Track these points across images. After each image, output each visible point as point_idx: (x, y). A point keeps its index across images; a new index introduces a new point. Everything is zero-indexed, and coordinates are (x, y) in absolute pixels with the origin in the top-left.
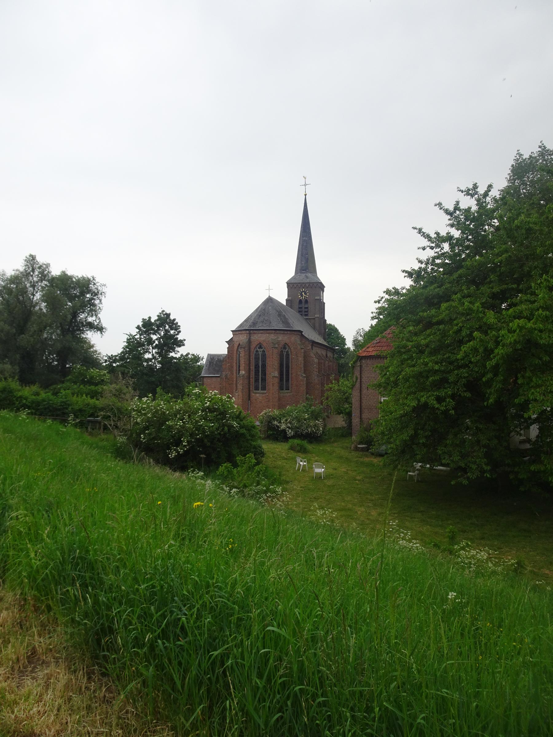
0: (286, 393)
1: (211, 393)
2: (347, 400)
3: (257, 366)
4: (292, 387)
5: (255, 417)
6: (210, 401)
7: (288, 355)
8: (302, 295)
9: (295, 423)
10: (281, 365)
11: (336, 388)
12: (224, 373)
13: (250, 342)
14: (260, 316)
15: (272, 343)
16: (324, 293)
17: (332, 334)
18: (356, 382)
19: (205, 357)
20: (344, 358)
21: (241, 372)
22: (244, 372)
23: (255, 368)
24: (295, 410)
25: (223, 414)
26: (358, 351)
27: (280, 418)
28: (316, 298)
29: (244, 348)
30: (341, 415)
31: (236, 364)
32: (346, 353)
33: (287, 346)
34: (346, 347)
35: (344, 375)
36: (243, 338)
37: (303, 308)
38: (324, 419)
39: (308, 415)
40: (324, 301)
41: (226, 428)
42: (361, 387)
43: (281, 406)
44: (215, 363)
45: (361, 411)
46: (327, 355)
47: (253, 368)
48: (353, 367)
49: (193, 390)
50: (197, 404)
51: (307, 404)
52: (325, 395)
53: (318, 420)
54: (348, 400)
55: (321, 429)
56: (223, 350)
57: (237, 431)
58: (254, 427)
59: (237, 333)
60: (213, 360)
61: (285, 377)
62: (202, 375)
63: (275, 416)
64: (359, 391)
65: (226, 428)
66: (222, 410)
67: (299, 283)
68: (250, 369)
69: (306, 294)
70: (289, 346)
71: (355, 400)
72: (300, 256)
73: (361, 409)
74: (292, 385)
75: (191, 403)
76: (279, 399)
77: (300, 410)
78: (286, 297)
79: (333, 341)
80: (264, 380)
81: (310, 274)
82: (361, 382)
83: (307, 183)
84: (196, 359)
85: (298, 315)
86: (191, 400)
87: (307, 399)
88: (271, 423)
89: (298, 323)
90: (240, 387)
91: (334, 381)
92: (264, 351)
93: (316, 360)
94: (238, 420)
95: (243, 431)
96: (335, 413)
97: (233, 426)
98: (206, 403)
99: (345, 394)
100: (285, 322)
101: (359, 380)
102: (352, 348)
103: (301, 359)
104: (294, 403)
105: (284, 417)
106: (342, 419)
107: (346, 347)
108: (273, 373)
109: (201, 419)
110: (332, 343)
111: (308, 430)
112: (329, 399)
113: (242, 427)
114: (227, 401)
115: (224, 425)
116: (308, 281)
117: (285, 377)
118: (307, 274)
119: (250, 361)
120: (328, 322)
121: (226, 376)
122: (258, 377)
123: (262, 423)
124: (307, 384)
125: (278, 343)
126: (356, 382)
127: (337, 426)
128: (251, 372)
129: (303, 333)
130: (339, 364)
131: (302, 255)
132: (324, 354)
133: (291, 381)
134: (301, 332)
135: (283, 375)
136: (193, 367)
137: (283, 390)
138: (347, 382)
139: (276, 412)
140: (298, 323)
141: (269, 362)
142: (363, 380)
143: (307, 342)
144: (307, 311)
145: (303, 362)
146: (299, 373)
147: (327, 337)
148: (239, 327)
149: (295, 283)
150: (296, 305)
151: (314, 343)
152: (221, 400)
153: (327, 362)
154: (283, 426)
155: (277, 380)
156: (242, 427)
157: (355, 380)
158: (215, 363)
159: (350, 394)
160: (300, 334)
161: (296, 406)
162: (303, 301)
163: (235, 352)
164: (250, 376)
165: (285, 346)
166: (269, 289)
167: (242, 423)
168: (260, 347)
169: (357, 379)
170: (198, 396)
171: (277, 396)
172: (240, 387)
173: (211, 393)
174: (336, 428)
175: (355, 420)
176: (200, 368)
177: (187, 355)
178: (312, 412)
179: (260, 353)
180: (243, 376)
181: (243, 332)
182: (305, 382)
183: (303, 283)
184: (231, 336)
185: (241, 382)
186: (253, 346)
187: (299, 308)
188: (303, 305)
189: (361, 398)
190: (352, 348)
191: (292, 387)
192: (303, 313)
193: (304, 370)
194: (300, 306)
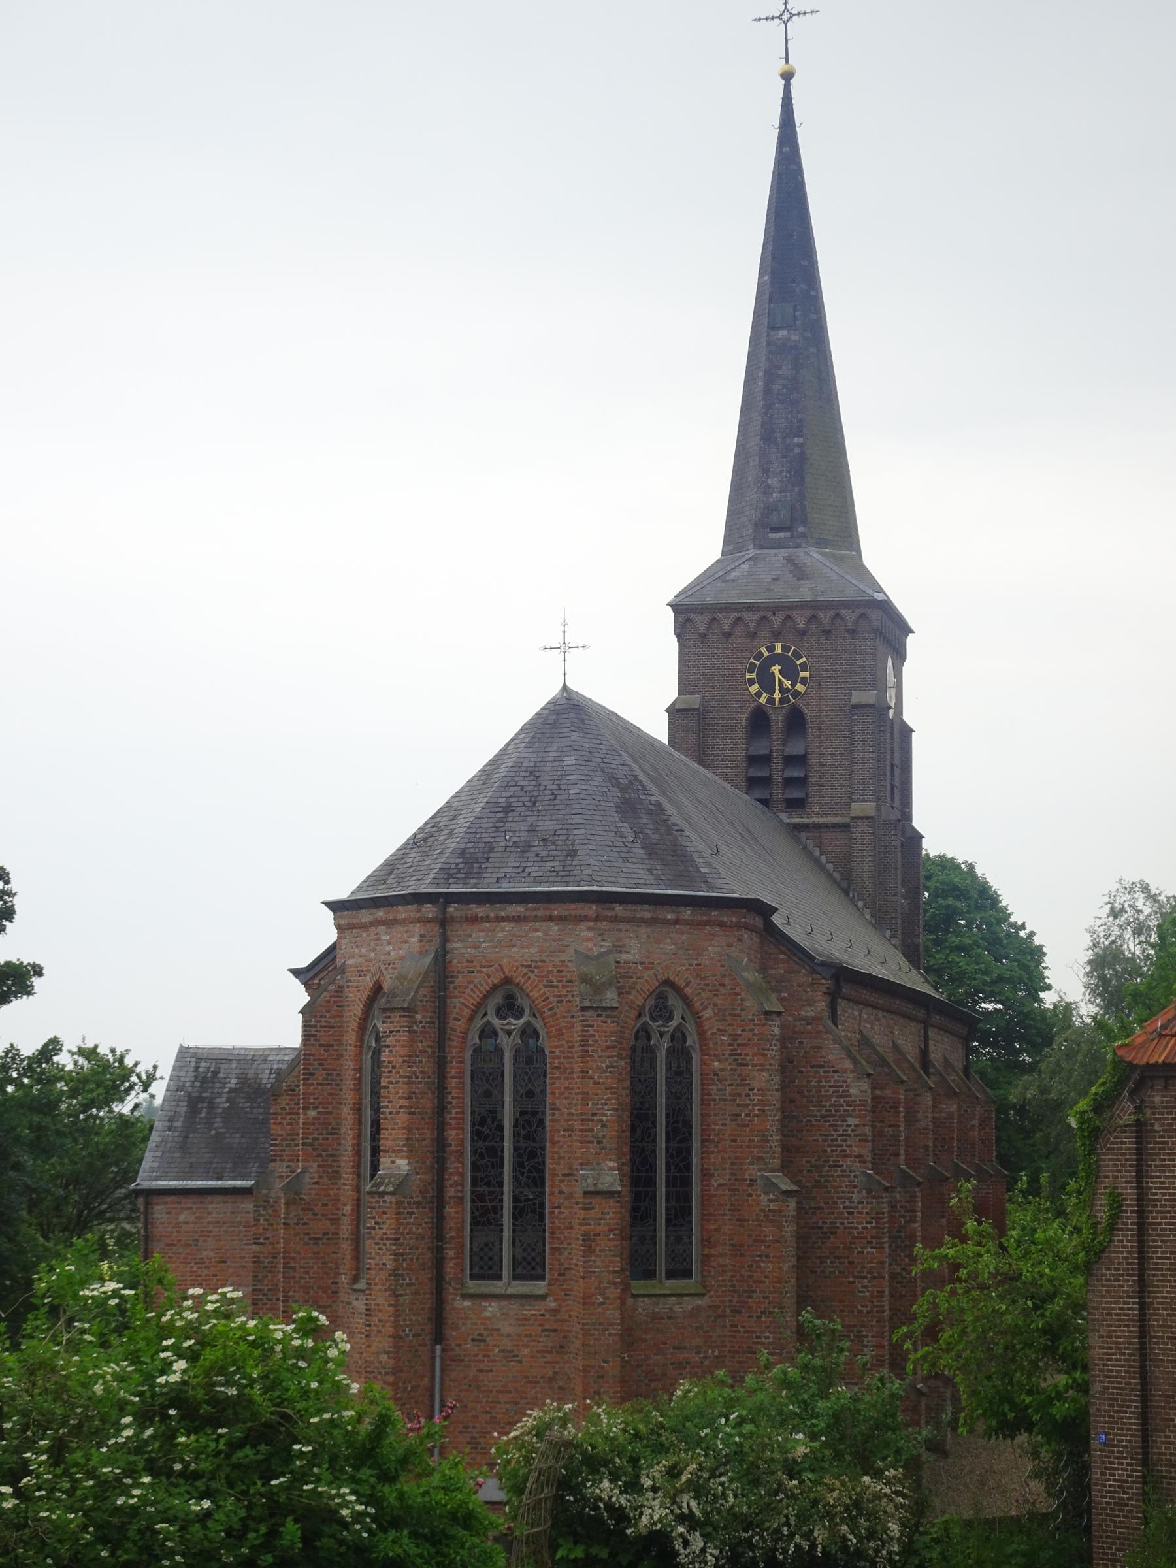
0: (672, 1300)
1: (200, 1301)
2: (1058, 1341)
3: (486, 1127)
4: (706, 1259)
5: (478, 1447)
6: (192, 1357)
7: (680, 1052)
8: (767, 682)
9: (730, 1494)
10: (639, 1121)
11: (989, 1263)
12: (280, 1168)
13: (441, 975)
14: (508, 810)
15: (585, 979)
16: (907, 669)
17: (951, 915)
18: (1112, 1227)
19: (165, 1071)
20: (1032, 1068)
21: (385, 1161)
22: (403, 1165)
23: (477, 1135)
24: (730, 1404)
25: (272, 1434)
26: (1126, 1030)
27: (634, 1461)
28: (858, 697)
29: (409, 1011)
30: (1023, 1438)
31: (358, 1109)
32: (1048, 1040)
33: (673, 1001)
34: (1049, 999)
35: (1034, 1179)
36: (401, 952)
37: (777, 761)
38: (913, 1466)
39: (813, 1437)
40: (907, 717)
41: (291, 1530)
42: (1142, 1259)
43: (638, 1384)
44: (222, 1103)
45: (1145, 1417)
46: (924, 1054)
47: (460, 1135)
48: (1094, 1135)
49: (84, 1283)
50: (108, 1374)
51: (806, 1368)
52: (921, 1307)
53: (877, 1474)
54: (1064, 1345)
55: (894, 1528)
56: (272, 1021)
57: (360, 1549)
58: (466, 1519)
59: (365, 916)
60: (211, 1081)
61: (661, 1189)
62: (144, 1181)
63: (603, 1447)
64: (1129, 1284)
65: (291, 1530)
66: (267, 1410)
67: (751, 607)
68: (441, 1143)
69: (790, 672)
70: (687, 1002)
71: (1106, 1342)
72: (754, 443)
73: (1144, 1398)
74: (706, 1242)
75: (69, 1364)
76: (629, 1336)
77: (761, 1409)
78: (671, 693)
79: (962, 961)
80: (531, 1212)
81: (815, 554)
82: (1142, 1227)
84: (107, 1076)
85: (744, 800)
86: (74, 1347)
87: (802, 1334)
88: (576, 1489)
89: (743, 857)
90: (380, 1258)
91: (970, 1225)
92: (529, 1033)
93: (859, 1090)
94: (365, 1473)
95: (398, 1544)
96: (981, 1427)
97: (332, 1515)
98: (166, 1368)
99: (1041, 1301)
100: (667, 848)
101: (1129, 1217)
102: (1087, 1010)
103: (764, 1079)
104: (719, 1362)
105: (661, 1449)
106: (1030, 1466)
107: (1049, 999)
108: (587, 1168)
109: (131, 1472)
110: (959, 979)
111: (808, 1536)
112: (946, 1335)
113: (388, 1521)
114: (300, 1353)
115: (276, 1509)
116: (804, 592)
117: (661, 1189)
118: (800, 553)
119: (441, 1090)
120: (932, 847)
121: (293, 1189)
122: (494, 1190)
123: (518, 1490)
124: (802, 1238)
125: (622, 979)
126: (1112, 1227)
127: (997, 1507)
128: (452, 1165)
129: (777, 919)
130: (1002, 1108)
131: (767, 437)
132: (909, 1044)
133: (705, 1217)
134: (763, 910)
135: (651, 1182)
136: (87, 1130)
137: (650, 1274)
138: (1053, 1229)
139: (611, 1420)
140: (743, 857)
142: (1154, 1216)
143: (803, 976)
144: (802, 782)
145: (775, 1098)
146: (752, 1171)
147: (924, 939)
148: (374, 880)
149: (727, 608)
150: (734, 746)
151: (844, 981)
152: (262, 1344)
153: (928, 1099)
154: (653, 1513)
155: (611, 1215)
156: (388, 1521)
157: (1103, 1217)
158: (222, 1103)
159: (1078, 1307)
160: (758, 922)
161: (737, 1379)
162: (777, 719)
163: (351, 1037)
164: (441, 1189)
165: (664, 997)
166: (564, 648)
167: (389, 1493)
168: (510, 1007)
169: (1115, 1217)
170: (116, 1322)
171: (613, 1314)
172: (380, 1258)
173: (200, 1301)
174: (990, 1523)
175: (1113, 1475)
176: (131, 1132)
177: (52, 1047)
178: (837, 1418)
179: (508, 1044)
180: (401, 1186)
181: (403, 912)
182: (789, 1229)
183: (775, 608)
184: (323, 933)
185: (388, 1226)
186: (461, 1003)
187: (752, 760)
188: (775, 744)
189: (1143, 1333)
190: (1087, 1010)
191: (706, 1259)
192: (778, 793)
193: (786, 1149)
194: (760, 748)
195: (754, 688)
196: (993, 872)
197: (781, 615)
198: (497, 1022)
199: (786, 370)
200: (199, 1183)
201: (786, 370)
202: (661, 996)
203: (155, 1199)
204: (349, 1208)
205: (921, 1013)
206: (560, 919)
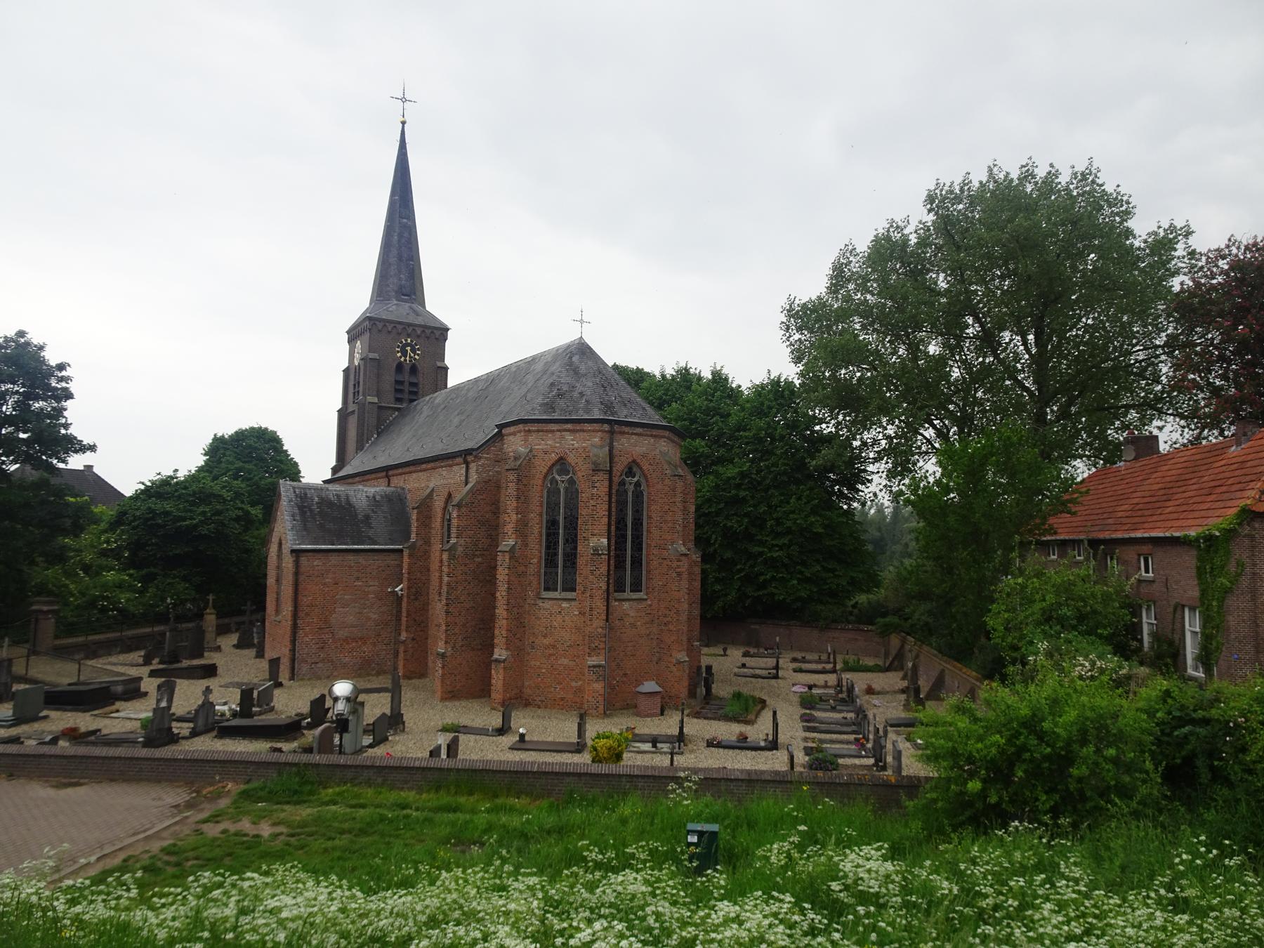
3: (552, 524)
7: (638, 495)
8: (404, 353)
37: (407, 384)
67: (400, 323)
69: (413, 351)
80: (571, 558)
108: (595, 540)
141: (654, 512)
179: (562, 487)
183: (410, 325)
187: (397, 382)
196: (280, 434)
198: (557, 477)
199: (406, 235)
201: (406, 235)
202: (630, 468)
204: (535, 561)
206: (655, 436)
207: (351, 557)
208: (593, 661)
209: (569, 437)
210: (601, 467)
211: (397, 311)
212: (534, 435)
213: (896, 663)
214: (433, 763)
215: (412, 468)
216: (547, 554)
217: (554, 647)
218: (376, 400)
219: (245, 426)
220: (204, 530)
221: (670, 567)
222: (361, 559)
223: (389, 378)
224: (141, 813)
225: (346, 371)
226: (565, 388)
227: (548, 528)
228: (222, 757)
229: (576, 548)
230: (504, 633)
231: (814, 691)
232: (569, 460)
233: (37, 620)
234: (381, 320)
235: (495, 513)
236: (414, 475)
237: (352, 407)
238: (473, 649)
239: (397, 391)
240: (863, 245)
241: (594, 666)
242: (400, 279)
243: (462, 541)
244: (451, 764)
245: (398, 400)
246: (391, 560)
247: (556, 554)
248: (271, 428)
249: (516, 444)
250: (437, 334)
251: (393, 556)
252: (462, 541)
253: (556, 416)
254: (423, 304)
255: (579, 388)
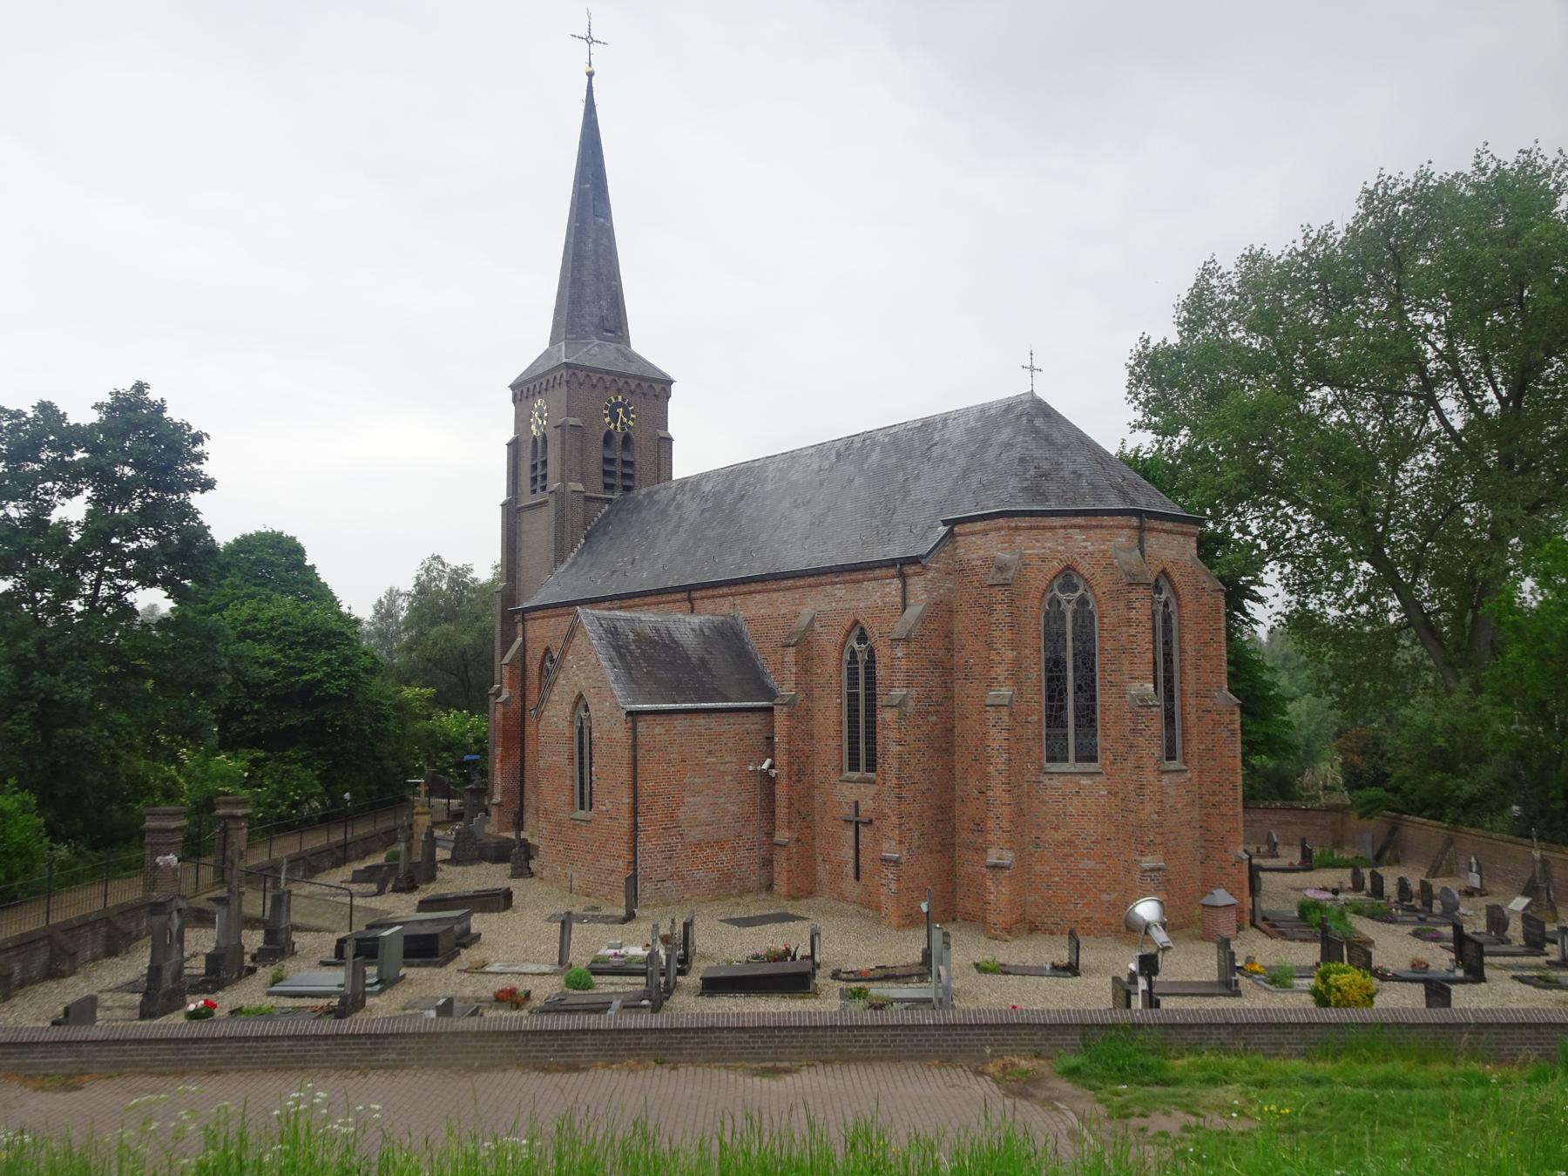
3: (1055, 666)
67: (608, 373)
69: (626, 414)
80: (1087, 717)
83: (585, 34)
92: (1083, 602)
179: (1069, 610)
183: (621, 375)
187: (607, 461)
194: (609, 455)
195: (607, 419)
197: (623, 380)
200: (690, 705)
203: (640, 718)
205: (685, 595)
207: (700, 721)
208: (1148, 862)
209: (1078, 536)
210: (1141, 579)
211: (596, 354)
212: (1024, 534)
213: (1388, 854)
214: (1122, 1016)
215: (758, 587)
216: (1050, 708)
217: (1070, 843)
218: (580, 487)
219: (250, 530)
220: (332, 688)
221: (1217, 723)
222: (713, 722)
223: (596, 453)
224: (1101, 1110)
225: (514, 447)
226: (1046, 466)
227: (1049, 670)
228: (734, 1022)
229: (1093, 698)
230: (1006, 825)
231: (1342, 896)
232: (1080, 569)
233: (225, 830)
234: (582, 368)
235: (948, 650)
236: (759, 597)
237: (527, 500)
238: (931, 852)
239: (607, 473)
240: (1229, 263)
241: (1152, 870)
242: (600, 308)
243: (913, 692)
244: (1151, 1016)
245: (609, 487)
246: (754, 723)
247: (1063, 708)
248: (288, 533)
249: (981, 547)
250: (654, 389)
251: (753, 717)
252: (913, 692)
253: (1053, 506)
254: (628, 344)
255: (1068, 468)
